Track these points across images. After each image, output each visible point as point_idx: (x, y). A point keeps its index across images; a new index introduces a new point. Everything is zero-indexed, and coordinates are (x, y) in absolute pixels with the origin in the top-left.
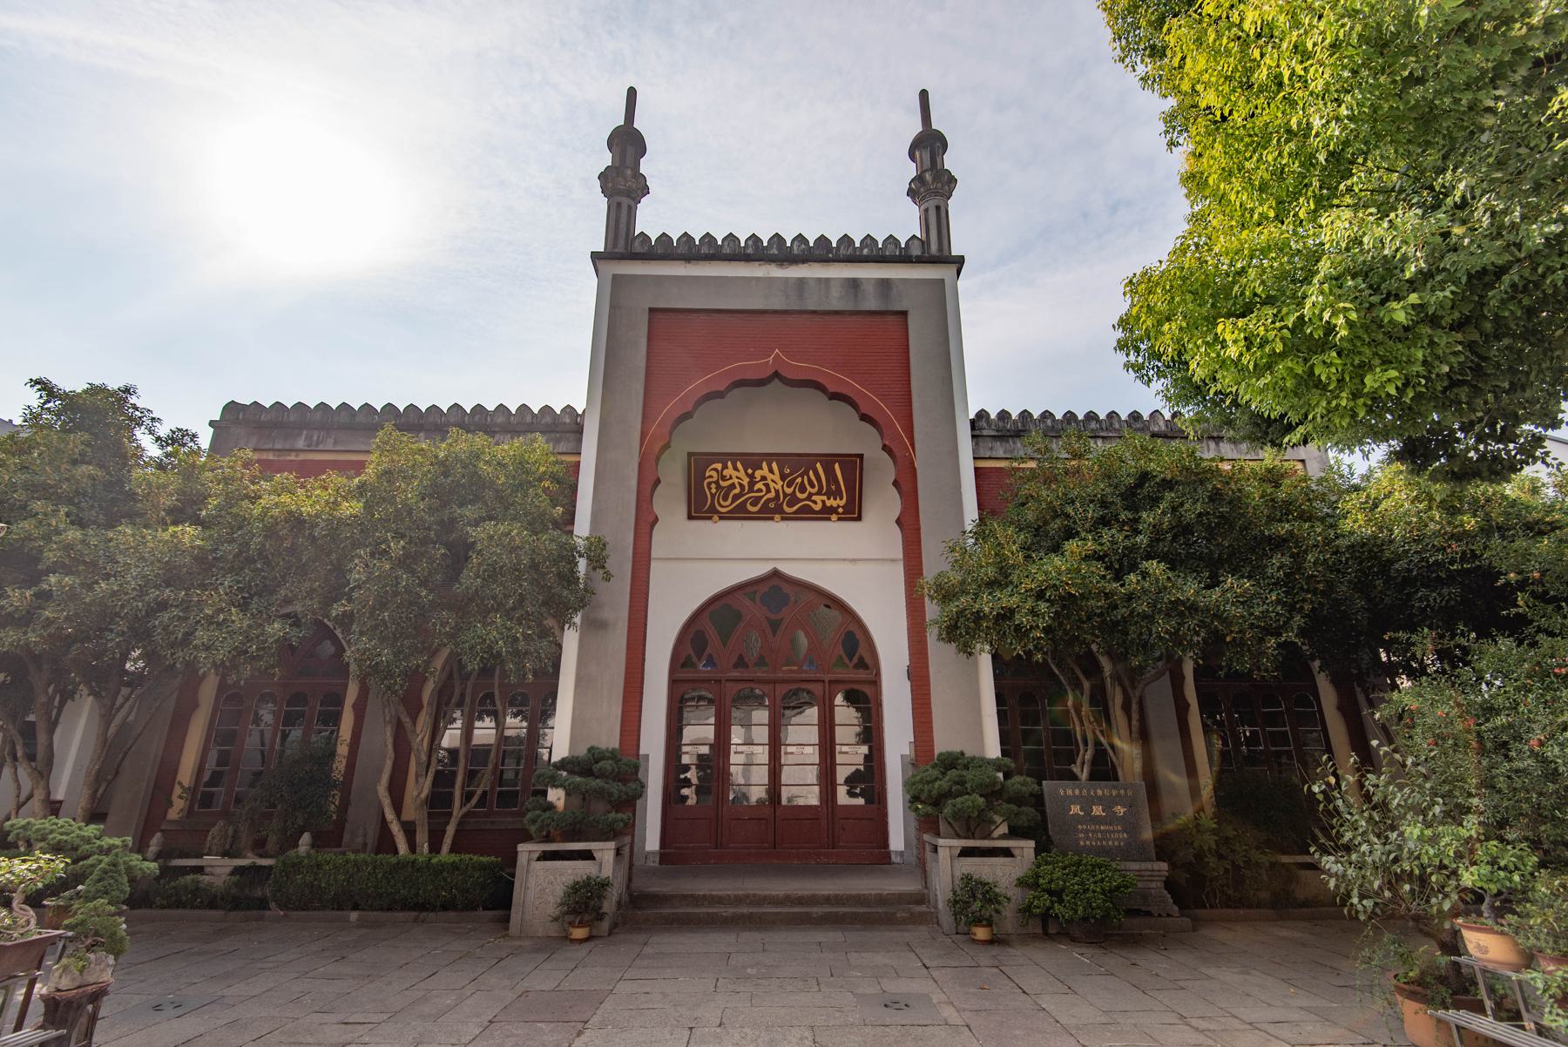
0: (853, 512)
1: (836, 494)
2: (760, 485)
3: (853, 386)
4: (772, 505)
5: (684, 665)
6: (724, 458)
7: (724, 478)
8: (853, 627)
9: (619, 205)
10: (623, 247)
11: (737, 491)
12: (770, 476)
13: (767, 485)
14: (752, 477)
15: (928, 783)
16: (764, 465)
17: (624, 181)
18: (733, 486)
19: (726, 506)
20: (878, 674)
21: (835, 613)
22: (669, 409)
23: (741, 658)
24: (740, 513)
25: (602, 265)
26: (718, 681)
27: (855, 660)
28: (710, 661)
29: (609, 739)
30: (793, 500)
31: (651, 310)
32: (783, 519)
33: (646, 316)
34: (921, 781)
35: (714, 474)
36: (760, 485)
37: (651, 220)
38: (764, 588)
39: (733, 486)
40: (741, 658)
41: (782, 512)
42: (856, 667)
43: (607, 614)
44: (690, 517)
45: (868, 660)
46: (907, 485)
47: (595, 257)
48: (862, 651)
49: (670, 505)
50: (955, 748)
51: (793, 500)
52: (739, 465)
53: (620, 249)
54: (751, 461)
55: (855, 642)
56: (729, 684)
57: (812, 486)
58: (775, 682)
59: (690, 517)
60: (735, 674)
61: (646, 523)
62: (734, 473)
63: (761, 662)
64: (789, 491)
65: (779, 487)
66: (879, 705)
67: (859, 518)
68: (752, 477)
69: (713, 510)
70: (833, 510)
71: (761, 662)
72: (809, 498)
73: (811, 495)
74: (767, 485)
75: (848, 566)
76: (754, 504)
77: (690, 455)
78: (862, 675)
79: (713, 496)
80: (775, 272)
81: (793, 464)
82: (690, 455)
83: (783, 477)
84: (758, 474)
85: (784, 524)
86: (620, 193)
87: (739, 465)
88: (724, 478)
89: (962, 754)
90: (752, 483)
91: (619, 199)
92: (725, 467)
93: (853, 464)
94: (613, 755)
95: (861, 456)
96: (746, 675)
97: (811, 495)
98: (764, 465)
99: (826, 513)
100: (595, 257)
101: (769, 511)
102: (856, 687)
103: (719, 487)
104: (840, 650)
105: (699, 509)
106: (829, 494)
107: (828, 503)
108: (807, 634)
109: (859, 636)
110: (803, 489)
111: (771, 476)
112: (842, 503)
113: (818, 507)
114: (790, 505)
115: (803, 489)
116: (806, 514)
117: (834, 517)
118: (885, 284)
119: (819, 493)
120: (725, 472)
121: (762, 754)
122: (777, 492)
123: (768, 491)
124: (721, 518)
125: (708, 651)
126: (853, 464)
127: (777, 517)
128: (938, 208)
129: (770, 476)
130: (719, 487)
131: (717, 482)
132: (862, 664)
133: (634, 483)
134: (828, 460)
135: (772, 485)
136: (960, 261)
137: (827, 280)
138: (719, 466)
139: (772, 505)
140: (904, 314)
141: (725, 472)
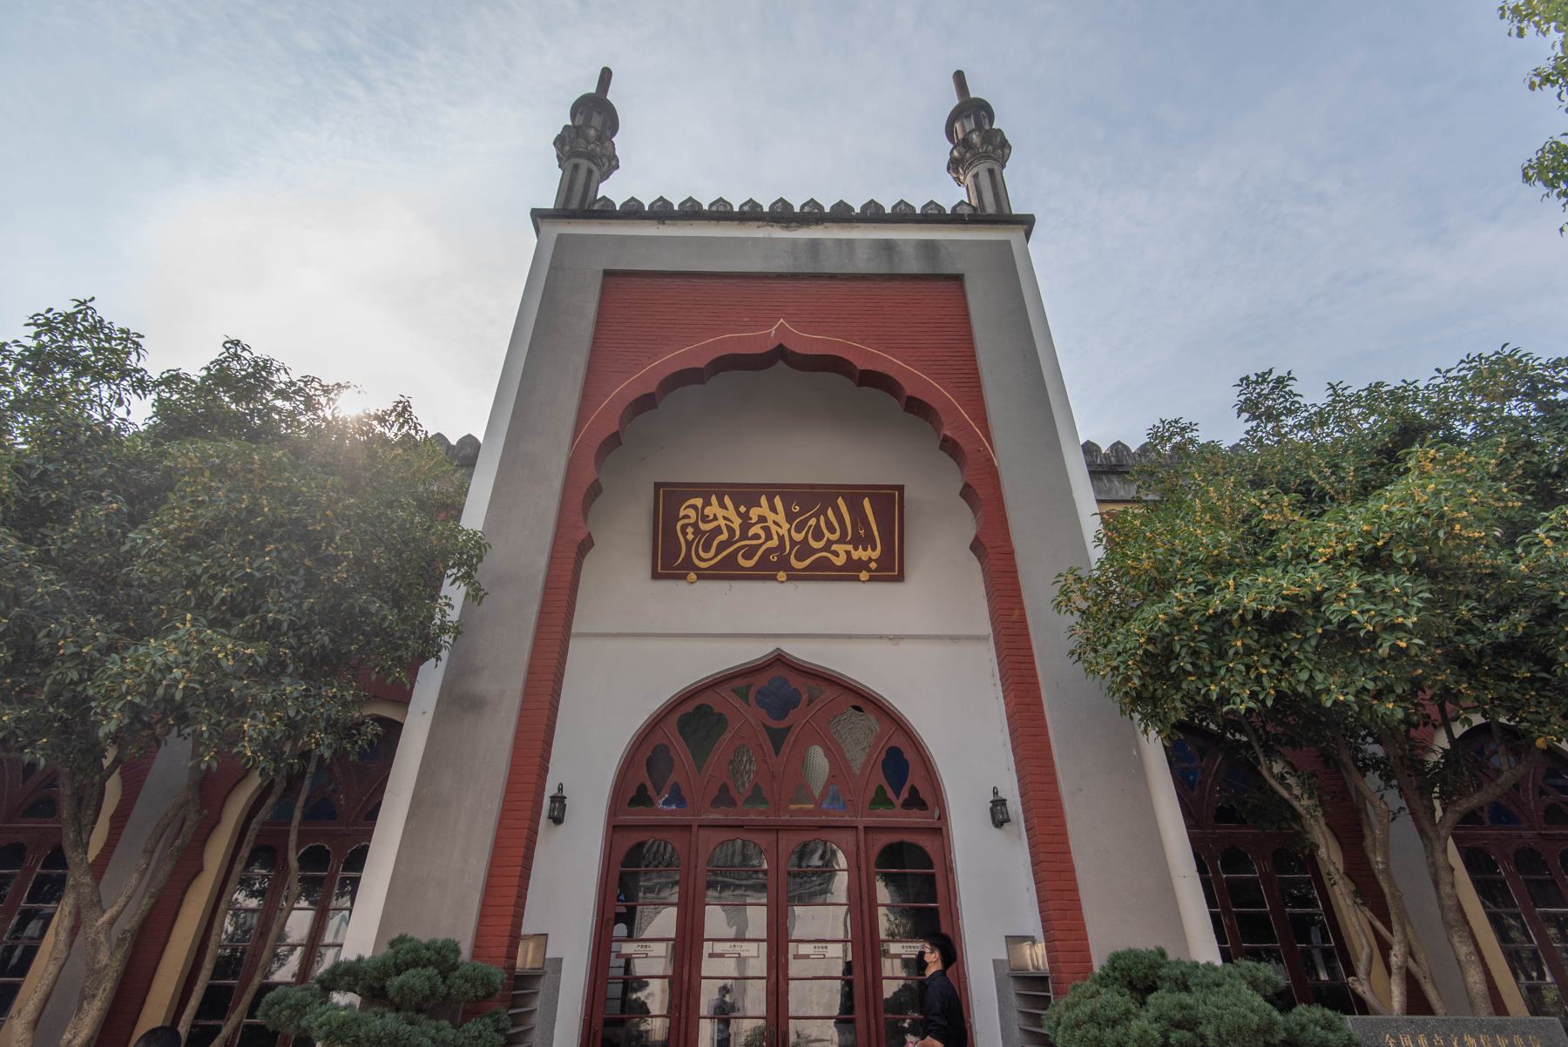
0: (891, 569)
1: (867, 541)
2: (756, 529)
3: (891, 362)
4: (774, 558)
5: (634, 802)
6: (706, 491)
7: (705, 519)
8: (899, 741)
9: (576, 167)
10: (577, 204)
11: (724, 536)
12: (771, 516)
13: (767, 530)
14: (745, 517)
15: (1113, 1023)
16: (763, 500)
17: (590, 133)
18: (718, 530)
19: (707, 559)
20: (943, 817)
21: (871, 720)
22: (625, 387)
23: (724, 789)
24: (727, 571)
25: (546, 227)
26: (687, 827)
27: (905, 794)
28: (677, 797)
29: (453, 920)
30: (804, 551)
31: (608, 274)
32: (790, 578)
33: (599, 278)
34: (1092, 1017)
35: (692, 513)
36: (756, 529)
37: (615, 190)
38: (761, 682)
39: (718, 530)
40: (724, 789)
41: (787, 567)
42: (907, 805)
43: (485, 685)
44: (656, 576)
45: (924, 793)
46: (983, 494)
47: (538, 216)
48: (915, 778)
49: (721, 983)
50: (1142, 941)
51: (804, 551)
52: (727, 500)
53: (574, 205)
54: (745, 495)
55: (904, 768)
56: (704, 834)
57: (832, 531)
58: (776, 829)
59: (656, 576)
60: (715, 816)
61: (571, 552)
62: (720, 513)
63: (756, 796)
64: (798, 537)
65: (783, 532)
66: (949, 870)
67: (900, 578)
68: (745, 517)
69: (688, 565)
70: (862, 565)
71: (756, 796)
72: (827, 548)
73: (830, 543)
74: (767, 530)
75: (886, 646)
76: (747, 557)
77: (658, 486)
78: (914, 818)
79: (689, 544)
80: (778, 233)
81: (806, 499)
82: (658, 486)
83: (790, 517)
84: (754, 513)
85: (791, 586)
86: (580, 155)
87: (727, 500)
88: (705, 519)
89: (1162, 954)
90: (745, 526)
91: (576, 161)
92: (707, 503)
93: (889, 500)
94: (670, 983)
95: (901, 488)
96: (732, 818)
97: (830, 543)
98: (763, 500)
99: (851, 571)
100: (538, 216)
101: (770, 567)
102: (908, 838)
103: (697, 531)
104: (879, 778)
105: (669, 563)
106: (857, 542)
107: (855, 555)
108: (828, 752)
109: (909, 755)
110: (818, 535)
111: (774, 519)
112: (876, 554)
113: (840, 561)
114: (800, 558)
115: (818, 535)
116: (823, 571)
117: (864, 575)
118: (930, 248)
119: (842, 540)
120: (708, 511)
121: (756, 957)
122: (781, 538)
123: (769, 537)
124: (701, 577)
125: (673, 778)
126: (889, 500)
127: (782, 575)
128: (991, 172)
129: (771, 516)
130: (697, 531)
131: (695, 525)
132: (914, 801)
133: (557, 484)
134: (854, 494)
135: (774, 528)
136: (1027, 222)
137: (850, 242)
138: (699, 502)
139: (774, 558)
140: (958, 279)
141: (708, 511)
